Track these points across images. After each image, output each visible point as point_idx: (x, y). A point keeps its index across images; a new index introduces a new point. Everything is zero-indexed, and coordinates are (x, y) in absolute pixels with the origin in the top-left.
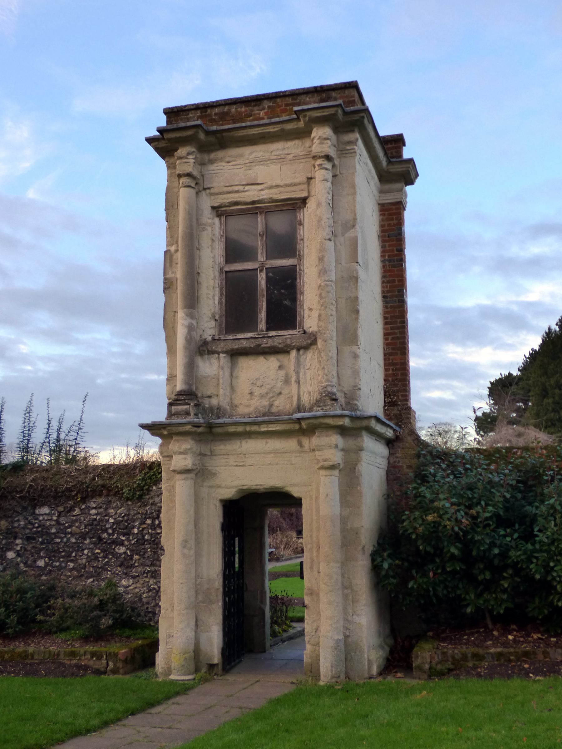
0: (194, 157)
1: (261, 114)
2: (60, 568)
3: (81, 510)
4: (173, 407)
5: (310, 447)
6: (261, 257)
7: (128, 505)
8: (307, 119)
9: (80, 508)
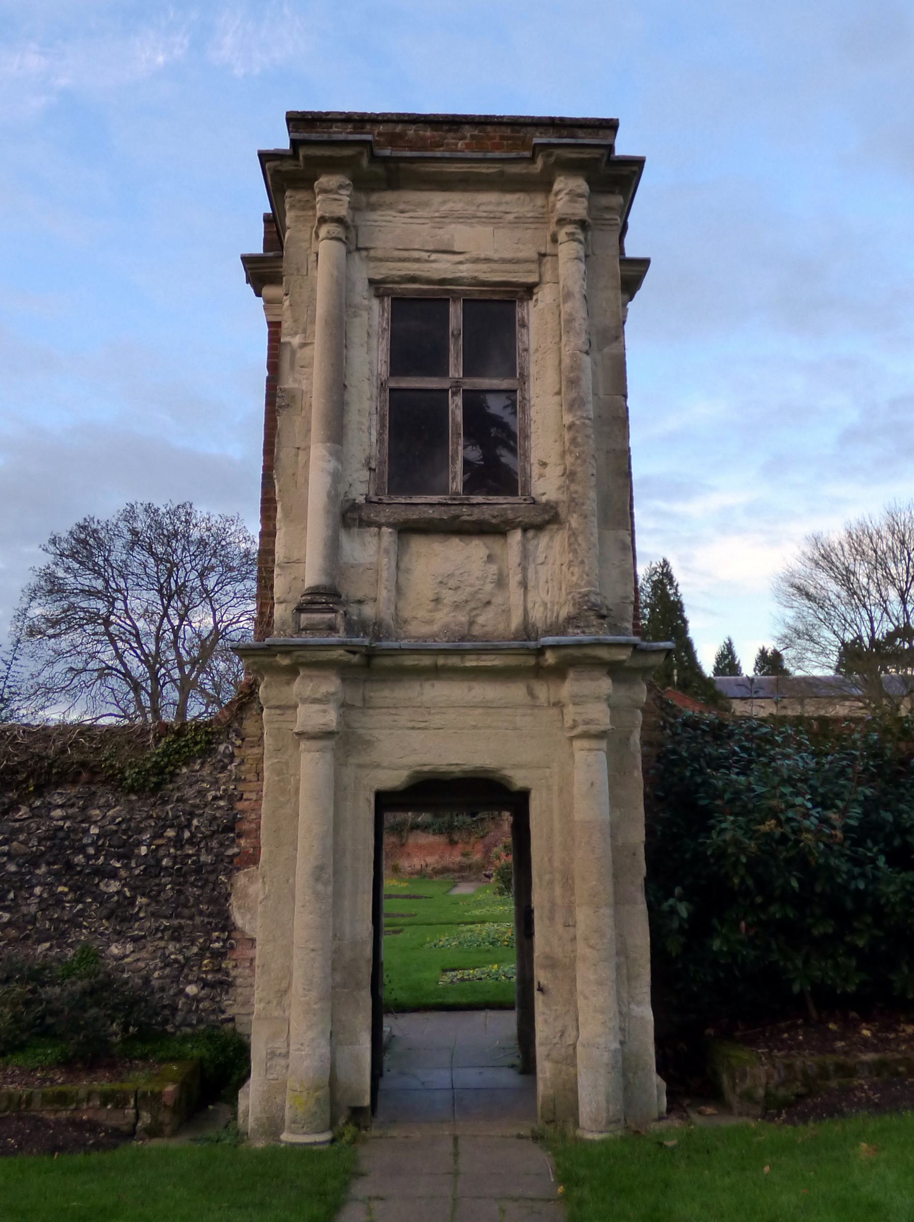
0: (348, 193)
1: (459, 145)
3: (32, 810)
4: (303, 616)
5: (549, 699)
6: (456, 369)
7: (130, 801)
8: (552, 159)
9: (30, 806)
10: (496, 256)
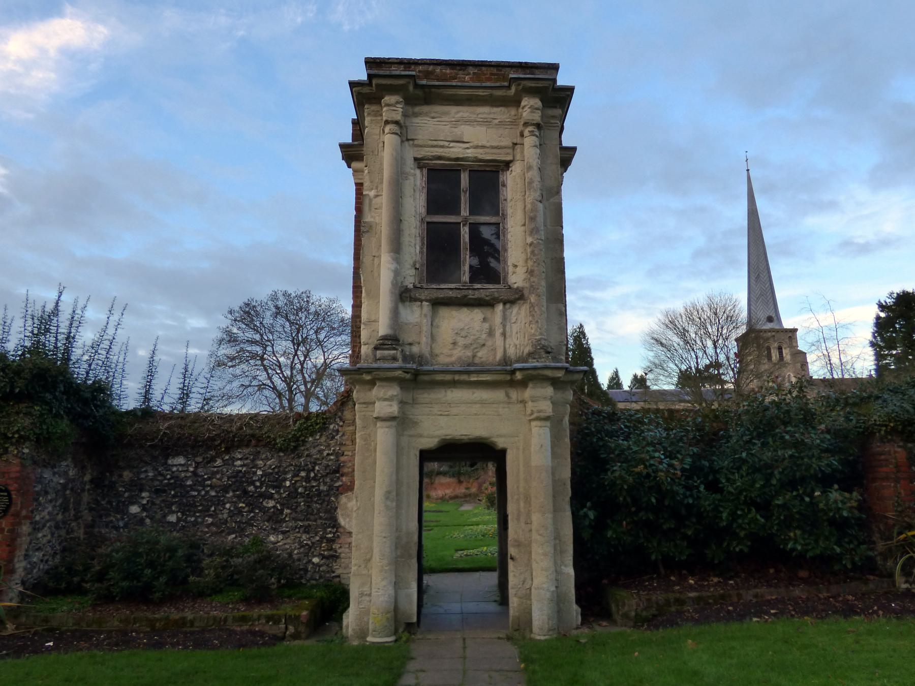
2: (195, 523)
3: (223, 461)
4: (378, 352)
6: (465, 211)
8: (521, 87)
10: (488, 145)
